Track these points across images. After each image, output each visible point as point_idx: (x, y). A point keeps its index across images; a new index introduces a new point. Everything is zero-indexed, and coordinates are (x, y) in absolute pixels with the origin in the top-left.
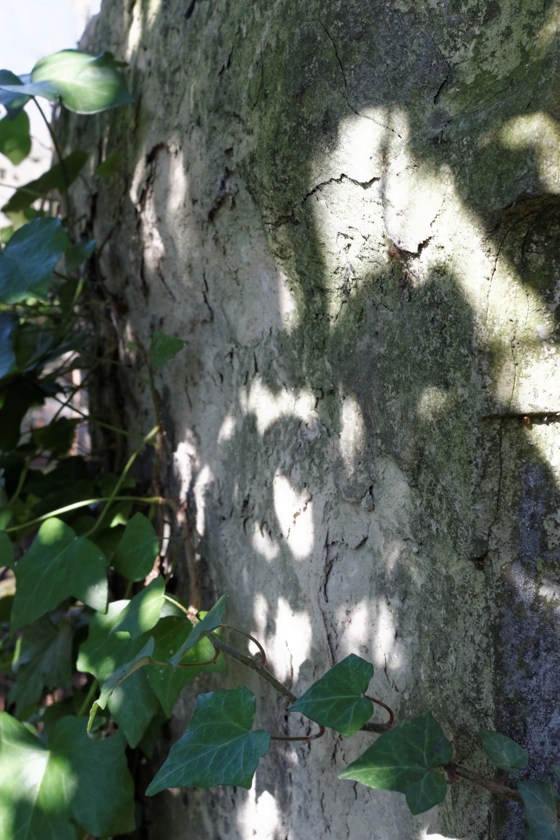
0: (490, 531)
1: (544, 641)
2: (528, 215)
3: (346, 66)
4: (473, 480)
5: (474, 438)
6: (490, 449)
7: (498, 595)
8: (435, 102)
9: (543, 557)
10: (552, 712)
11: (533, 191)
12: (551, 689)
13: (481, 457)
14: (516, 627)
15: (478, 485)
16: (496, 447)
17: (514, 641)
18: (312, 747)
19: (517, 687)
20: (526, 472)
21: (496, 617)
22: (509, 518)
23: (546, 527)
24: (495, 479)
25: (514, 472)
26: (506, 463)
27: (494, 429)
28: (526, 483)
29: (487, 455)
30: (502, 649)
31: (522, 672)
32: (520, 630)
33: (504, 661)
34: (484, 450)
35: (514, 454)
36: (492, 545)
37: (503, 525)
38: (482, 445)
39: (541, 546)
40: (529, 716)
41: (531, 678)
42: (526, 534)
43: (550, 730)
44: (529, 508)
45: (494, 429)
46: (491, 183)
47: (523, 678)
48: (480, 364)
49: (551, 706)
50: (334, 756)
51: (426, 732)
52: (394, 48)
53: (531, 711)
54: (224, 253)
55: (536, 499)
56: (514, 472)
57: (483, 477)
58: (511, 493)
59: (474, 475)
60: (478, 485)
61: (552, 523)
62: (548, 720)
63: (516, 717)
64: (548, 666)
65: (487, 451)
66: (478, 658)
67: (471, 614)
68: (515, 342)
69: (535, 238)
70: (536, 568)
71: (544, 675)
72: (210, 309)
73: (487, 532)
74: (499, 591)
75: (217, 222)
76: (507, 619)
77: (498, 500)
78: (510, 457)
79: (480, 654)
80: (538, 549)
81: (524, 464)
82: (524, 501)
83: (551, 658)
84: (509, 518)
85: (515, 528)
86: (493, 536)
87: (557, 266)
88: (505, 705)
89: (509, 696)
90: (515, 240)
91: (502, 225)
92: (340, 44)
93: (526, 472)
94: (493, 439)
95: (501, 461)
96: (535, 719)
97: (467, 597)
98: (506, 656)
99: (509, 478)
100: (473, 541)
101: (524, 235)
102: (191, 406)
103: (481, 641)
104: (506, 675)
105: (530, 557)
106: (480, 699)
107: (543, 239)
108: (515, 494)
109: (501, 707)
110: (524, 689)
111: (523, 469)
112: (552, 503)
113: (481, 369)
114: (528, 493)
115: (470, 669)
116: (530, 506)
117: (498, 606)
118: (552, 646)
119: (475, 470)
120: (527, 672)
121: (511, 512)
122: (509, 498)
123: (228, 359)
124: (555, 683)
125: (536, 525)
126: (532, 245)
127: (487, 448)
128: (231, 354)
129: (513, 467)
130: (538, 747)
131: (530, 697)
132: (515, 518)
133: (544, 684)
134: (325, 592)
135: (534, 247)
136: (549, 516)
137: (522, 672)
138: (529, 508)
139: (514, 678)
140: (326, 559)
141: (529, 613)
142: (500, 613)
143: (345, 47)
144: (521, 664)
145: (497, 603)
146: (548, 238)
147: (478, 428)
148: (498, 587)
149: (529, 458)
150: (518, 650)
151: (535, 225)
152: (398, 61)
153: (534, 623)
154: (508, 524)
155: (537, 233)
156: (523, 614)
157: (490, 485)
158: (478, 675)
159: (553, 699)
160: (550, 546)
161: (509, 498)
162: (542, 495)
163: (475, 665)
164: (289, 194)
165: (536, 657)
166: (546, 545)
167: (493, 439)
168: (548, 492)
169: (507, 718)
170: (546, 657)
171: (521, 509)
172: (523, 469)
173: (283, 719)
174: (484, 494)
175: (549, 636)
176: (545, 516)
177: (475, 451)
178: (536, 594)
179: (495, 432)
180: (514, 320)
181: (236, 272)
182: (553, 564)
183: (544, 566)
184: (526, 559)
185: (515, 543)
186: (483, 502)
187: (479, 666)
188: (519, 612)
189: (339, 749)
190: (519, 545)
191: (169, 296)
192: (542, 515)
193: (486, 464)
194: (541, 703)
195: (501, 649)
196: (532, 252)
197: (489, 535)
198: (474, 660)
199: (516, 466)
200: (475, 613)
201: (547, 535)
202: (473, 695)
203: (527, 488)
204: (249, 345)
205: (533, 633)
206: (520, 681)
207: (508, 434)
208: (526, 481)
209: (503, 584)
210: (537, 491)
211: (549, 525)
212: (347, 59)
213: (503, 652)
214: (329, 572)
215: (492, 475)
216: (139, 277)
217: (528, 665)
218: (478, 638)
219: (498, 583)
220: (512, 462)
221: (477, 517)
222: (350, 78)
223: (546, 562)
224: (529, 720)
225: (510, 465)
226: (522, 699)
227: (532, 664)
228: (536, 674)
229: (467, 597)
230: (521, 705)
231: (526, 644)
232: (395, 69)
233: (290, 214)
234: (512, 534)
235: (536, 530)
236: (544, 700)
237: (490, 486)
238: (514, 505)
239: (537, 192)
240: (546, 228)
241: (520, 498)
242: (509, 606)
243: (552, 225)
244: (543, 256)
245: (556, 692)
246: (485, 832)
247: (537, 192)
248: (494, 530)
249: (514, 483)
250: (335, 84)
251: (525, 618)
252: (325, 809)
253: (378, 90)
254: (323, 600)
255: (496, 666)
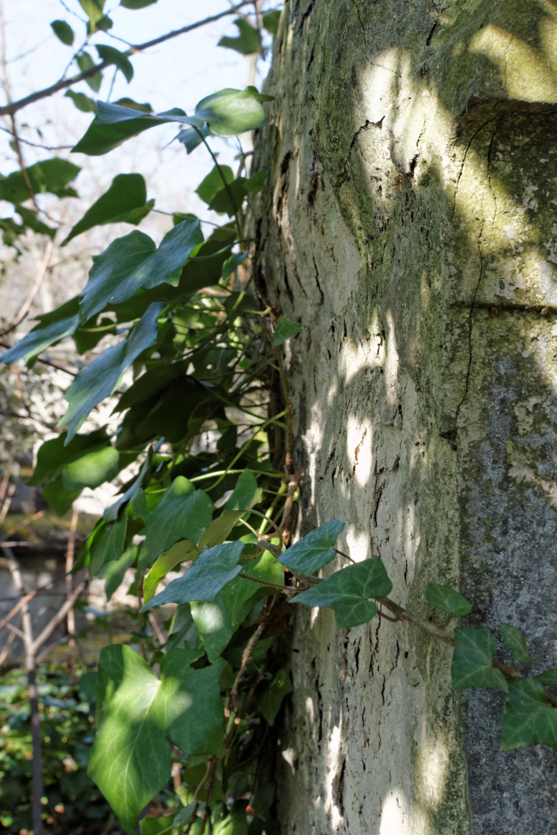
0: (458, 409)
1: (513, 520)
2: (487, 123)
3: (366, 27)
4: (443, 363)
5: (444, 324)
6: (459, 335)
7: (465, 470)
8: (428, 44)
9: (513, 441)
10: (520, 589)
11: (480, 95)
12: (520, 567)
13: (450, 341)
14: (484, 502)
15: (447, 367)
16: (466, 334)
17: (480, 515)
18: (360, 666)
19: (484, 559)
20: (497, 360)
21: (463, 490)
22: (478, 400)
23: (517, 413)
24: (465, 363)
25: (484, 359)
26: (475, 350)
27: (464, 318)
28: (496, 370)
29: (456, 341)
30: (468, 521)
31: (490, 546)
32: (488, 505)
33: (469, 531)
34: (453, 335)
35: (484, 342)
36: (460, 423)
37: (472, 406)
38: (451, 331)
39: (511, 430)
40: (496, 589)
41: (498, 553)
42: (495, 417)
43: (518, 607)
44: (499, 393)
45: (464, 318)
46: (452, 96)
47: (489, 551)
48: (446, 256)
49: (520, 583)
50: (371, 666)
51: (371, 571)
52: (399, 5)
53: (498, 584)
54: (323, 233)
55: (507, 386)
56: (484, 359)
57: (452, 360)
58: (481, 377)
59: (444, 358)
60: (447, 367)
61: (524, 411)
62: (516, 596)
63: (482, 587)
64: (517, 544)
65: (456, 337)
66: (450, 531)
67: (448, 493)
68: (481, 239)
69: (501, 147)
70: (505, 450)
71: (512, 552)
72: (321, 291)
73: (455, 410)
74: (467, 466)
75: (316, 205)
76: (474, 493)
77: (467, 382)
78: (480, 344)
79: (452, 528)
80: (508, 432)
81: (494, 352)
82: (493, 387)
83: (520, 537)
84: (478, 400)
85: (484, 410)
86: (461, 414)
87: (525, 175)
88: (469, 574)
89: (475, 566)
90: (480, 148)
91: (464, 133)
92: (361, 9)
93: (497, 360)
94: (462, 326)
95: (471, 347)
96: (501, 592)
97: (446, 479)
98: (472, 527)
99: (478, 364)
100: (442, 417)
101: (488, 143)
102: (316, 391)
103: (453, 515)
104: (472, 545)
105: (499, 439)
106: (449, 569)
107: (509, 148)
108: (485, 379)
109: (466, 574)
110: (489, 562)
111: (493, 357)
112: (523, 392)
113: (446, 260)
114: (499, 379)
115: (443, 542)
116: (499, 391)
117: (464, 480)
118: (522, 525)
119: (445, 353)
120: (494, 546)
121: (481, 395)
122: (478, 382)
123: (331, 333)
124: (525, 562)
125: (506, 410)
126: (498, 154)
127: (456, 334)
128: (333, 328)
129: (483, 354)
130: (505, 620)
131: (497, 571)
132: (484, 400)
133: (512, 561)
134: (375, 518)
135: (501, 156)
136: (520, 404)
137: (490, 546)
138: (499, 393)
139: (480, 550)
140: (376, 486)
141: (497, 491)
142: (467, 486)
143: (365, 10)
144: (488, 538)
145: (464, 477)
146: (514, 148)
147: (448, 314)
148: (465, 462)
149: (500, 348)
150: (485, 524)
151: (498, 134)
152: (402, 15)
153: (503, 501)
154: (477, 405)
155: (502, 142)
156: (491, 491)
157: (459, 368)
158: (449, 547)
159: (522, 576)
160: (521, 432)
161: (478, 382)
162: (514, 383)
163: (447, 538)
164: (340, 152)
165: (504, 533)
166: (517, 430)
167: (462, 326)
168: (520, 381)
169: (472, 586)
170: (514, 536)
171: (491, 394)
172: (493, 357)
173: (343, 646)
174: (452, 375)
175: (518, 516)
176: (517, 403)
177: (445, 336)
178: (506, 474)
179: (464, 320)
180: (481, 219)
181: (332, 249)
182: (523, 448)
183: (514, 450)
184: (495, 440)
185: (484, 424)
186: (452, 383)
187: (450, 538)
188: (487, 488)
189: (375, 661)
190: (489, 426)
191: (303, 294)
192: (512, 402)
193: (455, 349)
194: (509, 578)
195: (467, 521)
196: (499, 160)
197: (457, 414)
198: (447, 533)
199: (486, 354)
200: (451, 492)
201: (517, 421)
202: (445, 565)
203: (497, 375)
204: (341, 314)
205: (501, 511)
206: (486, 553)
207: (478, 324)
208: (497, 369)
209: (471, 461)
210: (508, 379)
211: (520, 412)
212: (367, 21)
213: (469, 523)
214: (379, 499)
215: (461, 359)
216: (283, 282)
217: (495, 540)
218: (451, 513)
219: (466, 459)
220: (482, 350)
221: (446, 396)
222: (368, 36)
223: (516, 446)
224: (496, 592)
225: (480, 352)
226: (488, 571)
227: (500, 539)
228: (504, 550)
229: (446, 479)
230: (487, 577)
231: (493, 520)
232: (399, 22)
233: (343, 171)
234: (481, 415)
235: (506, 414)
236: (512, 576)
237: (459, 369)
238: (483, 388)
239: (484, 96)
240: (509, 138)
241: (490, 383)
242: (477, 481)
243: (515, 135)
244: (510, 164)
245: (526, 571)
246: (450, 695)
247: (484, 96)
248: (463, 409)
249: (484, 368)
250: (358, 43)
251: (494, 495)
252: (366, 724)
253: (387, 41)
254: (372, 526)
255: (462, 535)
